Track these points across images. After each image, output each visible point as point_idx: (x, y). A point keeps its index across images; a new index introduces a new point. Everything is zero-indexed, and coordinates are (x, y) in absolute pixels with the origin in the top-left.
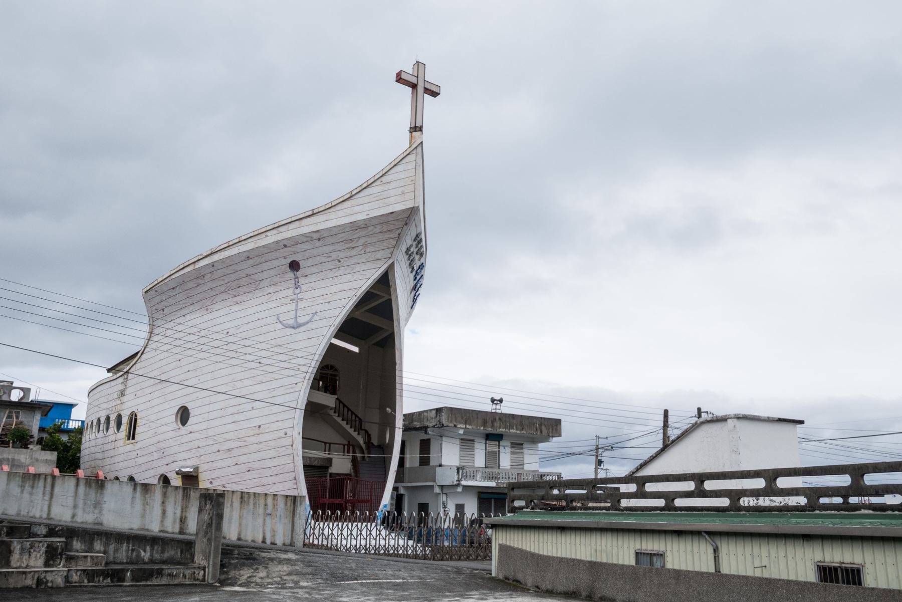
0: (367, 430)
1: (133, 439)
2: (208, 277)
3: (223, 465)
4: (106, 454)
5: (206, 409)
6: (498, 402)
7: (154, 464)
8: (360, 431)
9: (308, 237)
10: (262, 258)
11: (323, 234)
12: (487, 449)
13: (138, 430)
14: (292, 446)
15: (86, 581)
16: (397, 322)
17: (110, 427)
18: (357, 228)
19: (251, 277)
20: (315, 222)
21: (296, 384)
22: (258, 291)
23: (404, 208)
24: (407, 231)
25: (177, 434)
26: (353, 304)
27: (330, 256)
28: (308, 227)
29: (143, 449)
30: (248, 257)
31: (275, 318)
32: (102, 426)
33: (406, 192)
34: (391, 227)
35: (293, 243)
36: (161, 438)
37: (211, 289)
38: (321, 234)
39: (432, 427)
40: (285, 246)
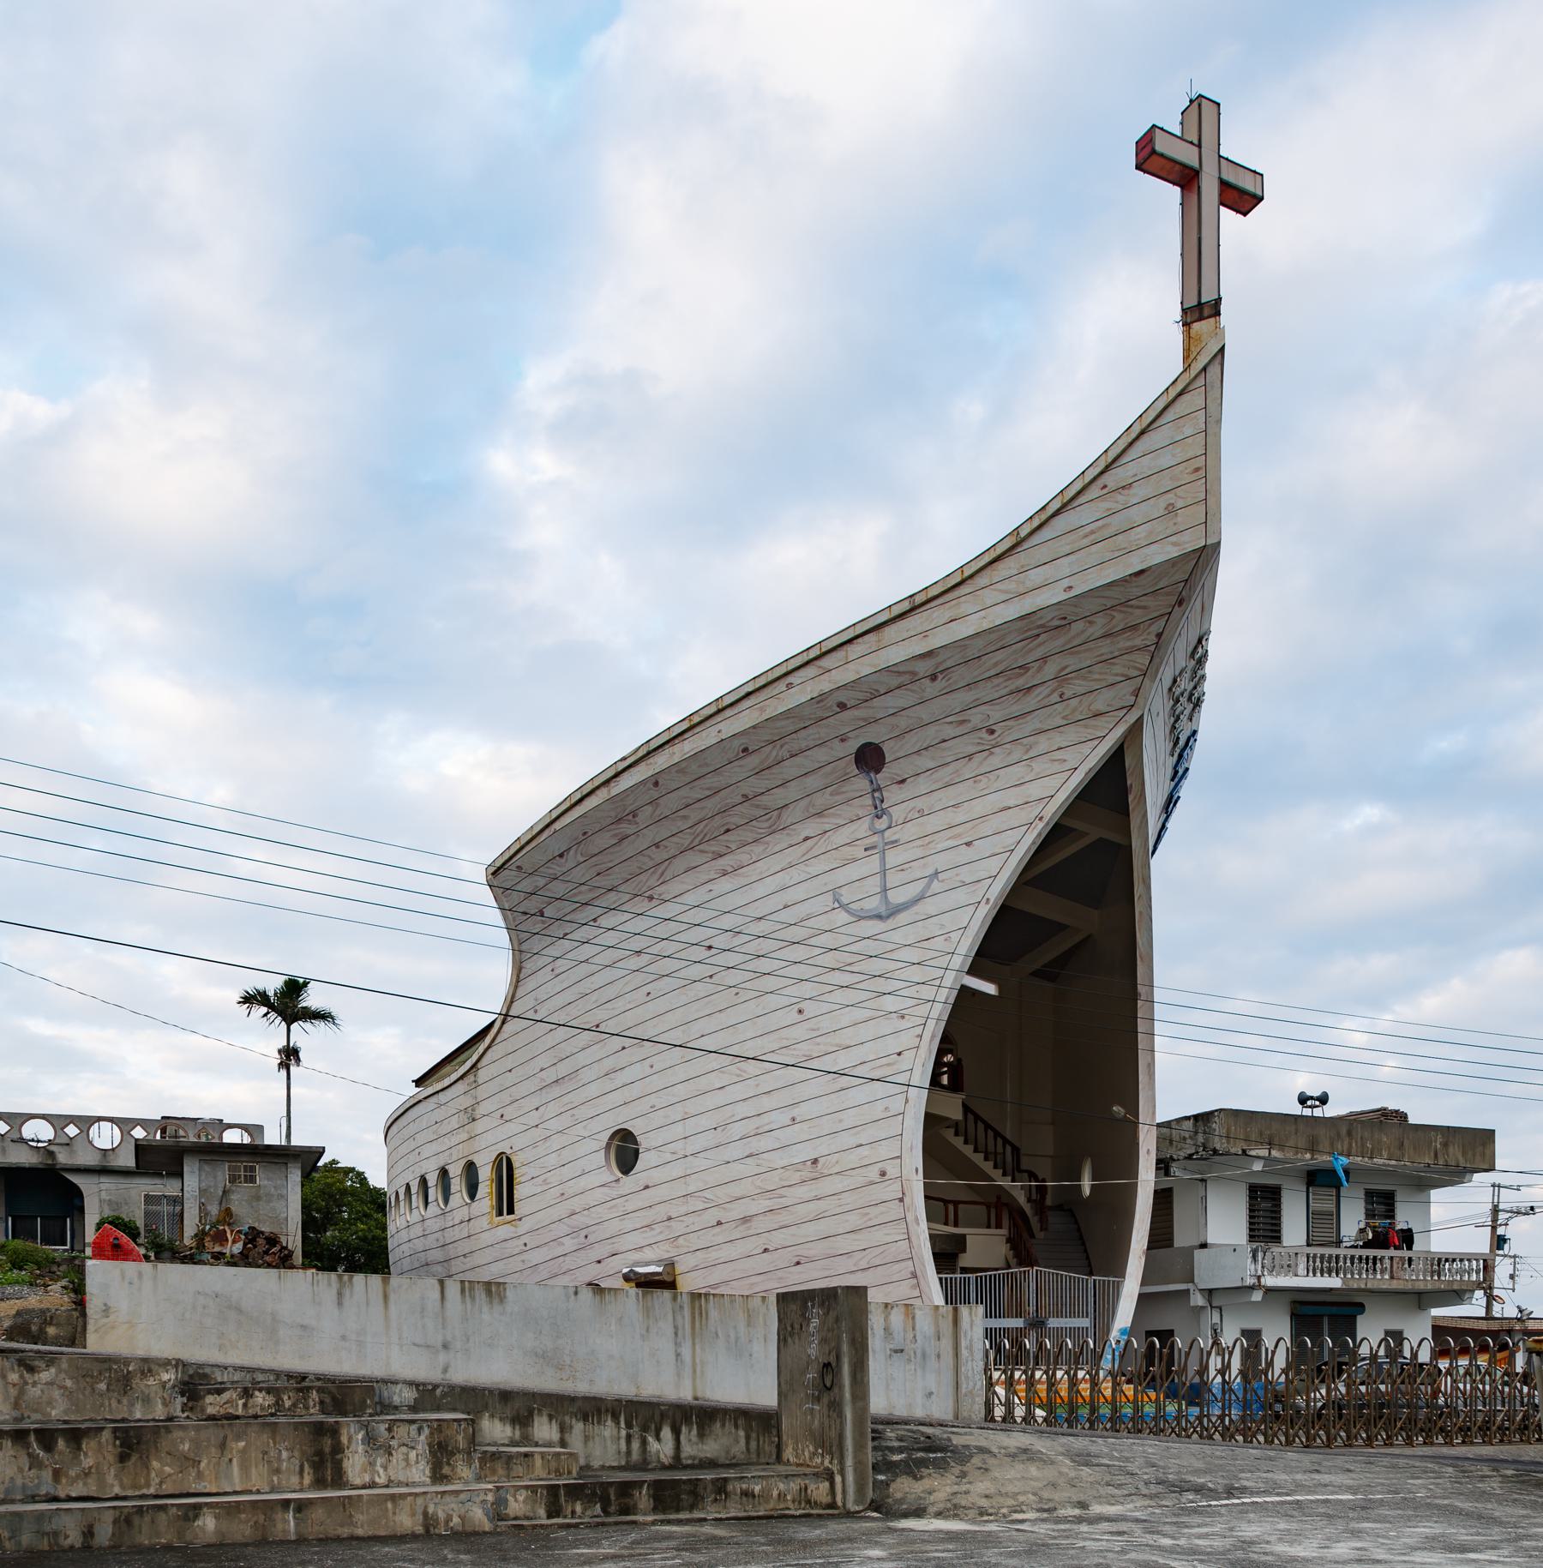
0: (1033, 1170)
1: (511, 1211)
2: (645, 815)
3: (734, 1256)
4: (452, 1251)
5: (678, 1130)
6: (1317, 1103)
7: (569, 1263)
8: (1016, 1173)
9: (904, 673)
10: (782, 746)
11: (945, 661)
12: (1311, 1204)
13: (519, 1192)
14: (901, 1200)
15: (542, 1512)
16: (1141, 886)
17: (452, 1191)
18: (1036, 632)
19: (754, 801)
20: (920, 630)
21: (899, 1054)
22: (777, 836)
23: (1174, 552)
24: (1183, 620)
25: (614, 1193)
26: (1034, 843)
27: (964, 721)
28: (899, 648)
29: (538, 1232)
30: (745, 750)
31: (829, 897)
32: (432, 1192)
33: (1180, 504)
34: (1138, 616)
35: (862, 696)
36: (576, 1203)
37: (657, 845)
38: (939, 659)
39: (1186, 1158)
40: (842, 706)
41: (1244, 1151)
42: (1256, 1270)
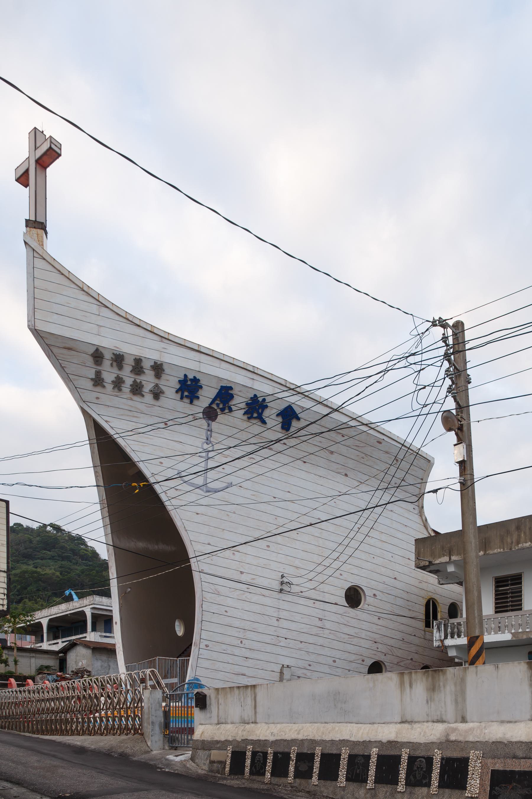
41: (430, 562)
42: (440, 636)
